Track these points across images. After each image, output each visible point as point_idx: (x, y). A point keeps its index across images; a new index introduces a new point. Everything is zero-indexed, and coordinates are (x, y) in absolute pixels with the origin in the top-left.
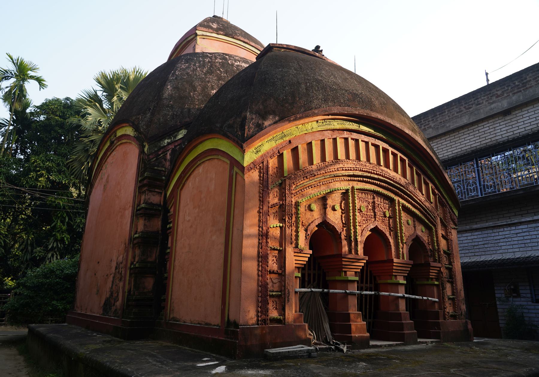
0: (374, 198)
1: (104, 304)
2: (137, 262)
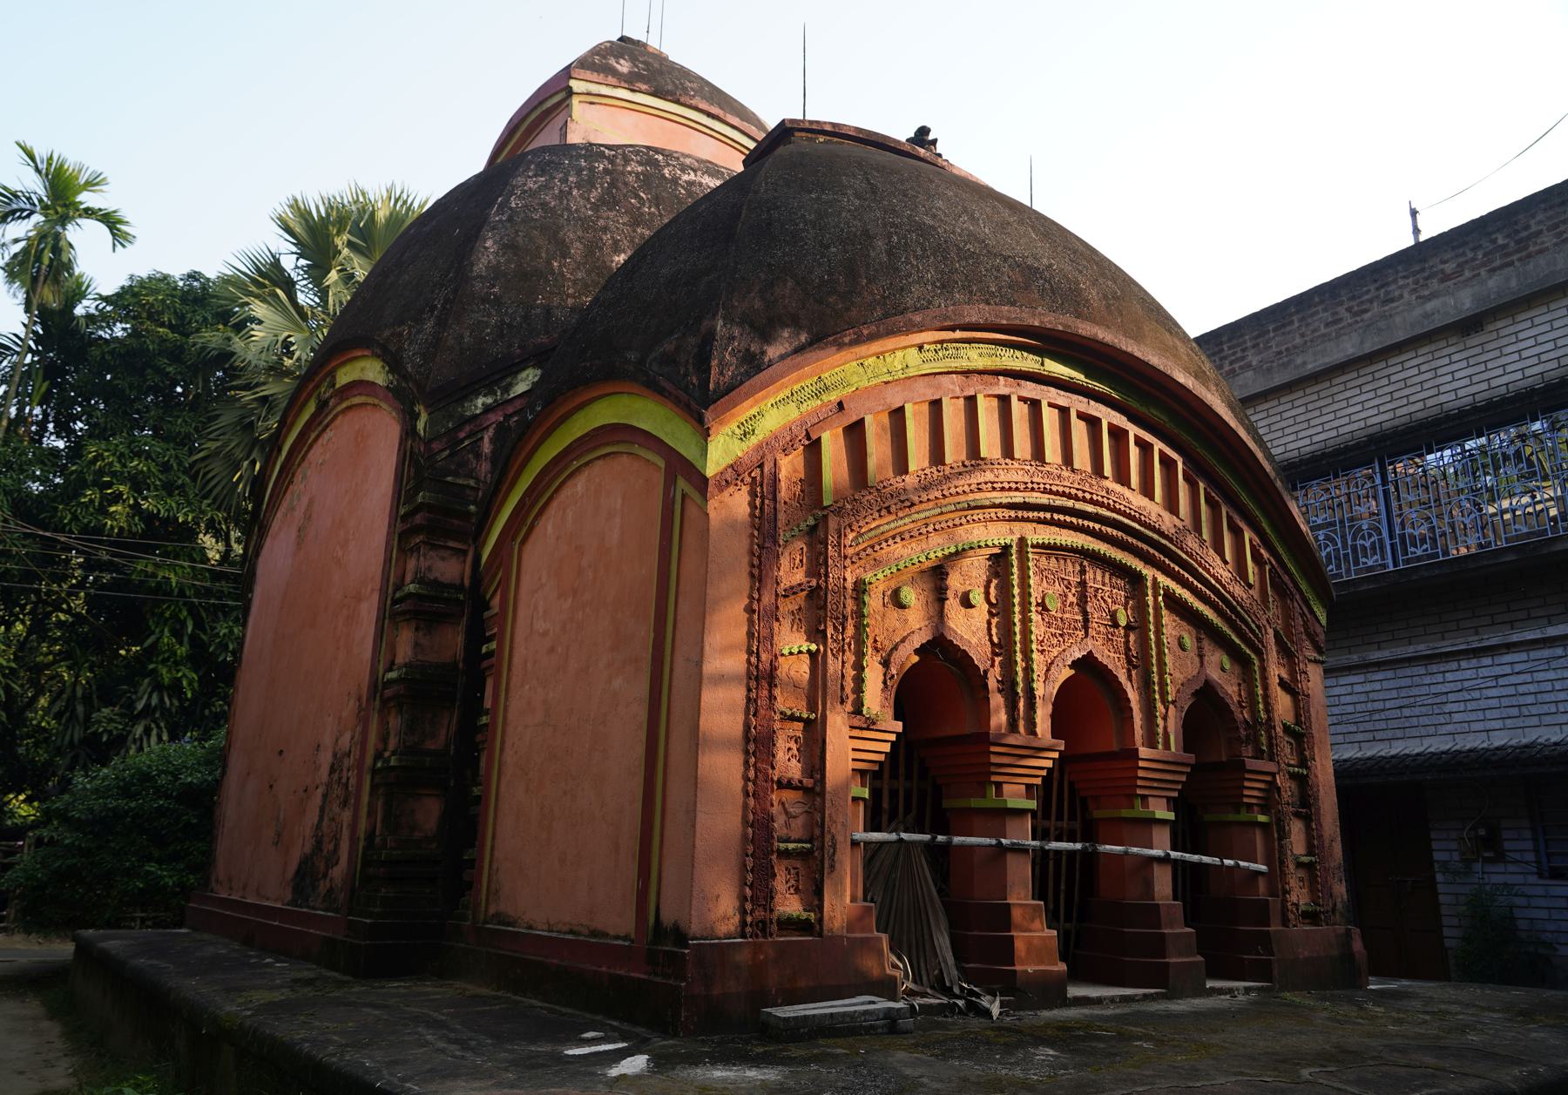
0: (1083, 572)
1: (298, 872)
2: (394, 753)
